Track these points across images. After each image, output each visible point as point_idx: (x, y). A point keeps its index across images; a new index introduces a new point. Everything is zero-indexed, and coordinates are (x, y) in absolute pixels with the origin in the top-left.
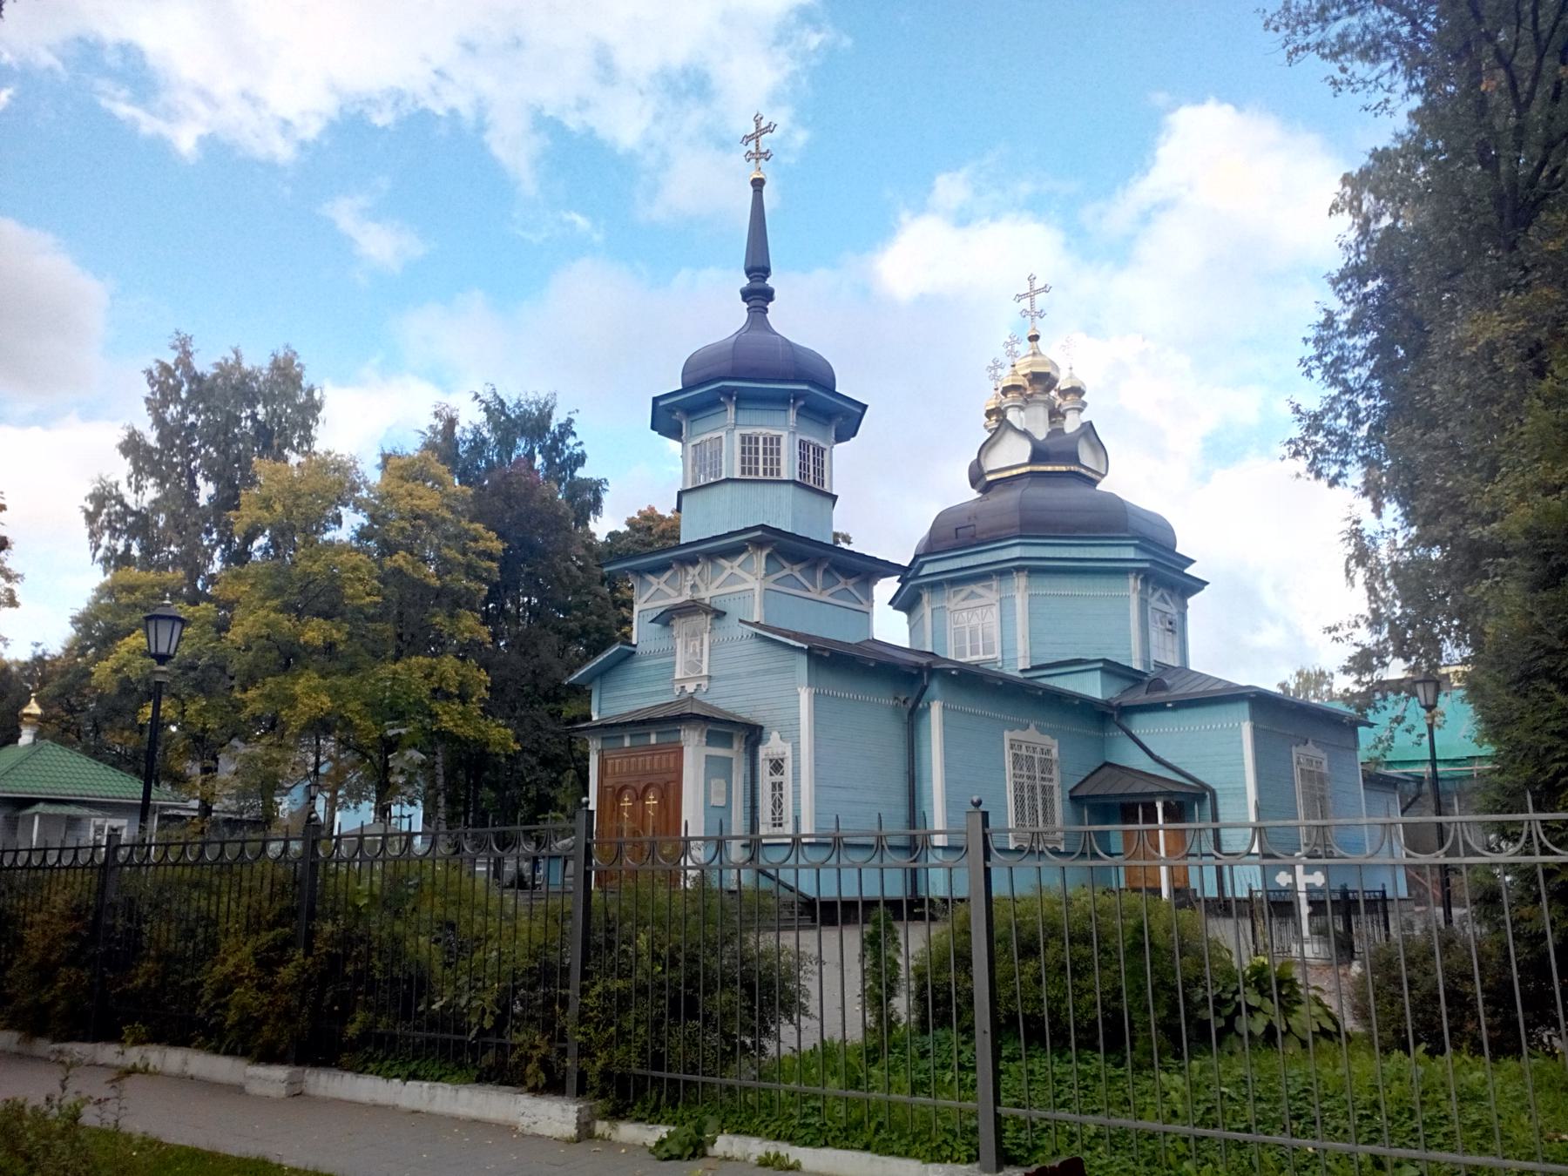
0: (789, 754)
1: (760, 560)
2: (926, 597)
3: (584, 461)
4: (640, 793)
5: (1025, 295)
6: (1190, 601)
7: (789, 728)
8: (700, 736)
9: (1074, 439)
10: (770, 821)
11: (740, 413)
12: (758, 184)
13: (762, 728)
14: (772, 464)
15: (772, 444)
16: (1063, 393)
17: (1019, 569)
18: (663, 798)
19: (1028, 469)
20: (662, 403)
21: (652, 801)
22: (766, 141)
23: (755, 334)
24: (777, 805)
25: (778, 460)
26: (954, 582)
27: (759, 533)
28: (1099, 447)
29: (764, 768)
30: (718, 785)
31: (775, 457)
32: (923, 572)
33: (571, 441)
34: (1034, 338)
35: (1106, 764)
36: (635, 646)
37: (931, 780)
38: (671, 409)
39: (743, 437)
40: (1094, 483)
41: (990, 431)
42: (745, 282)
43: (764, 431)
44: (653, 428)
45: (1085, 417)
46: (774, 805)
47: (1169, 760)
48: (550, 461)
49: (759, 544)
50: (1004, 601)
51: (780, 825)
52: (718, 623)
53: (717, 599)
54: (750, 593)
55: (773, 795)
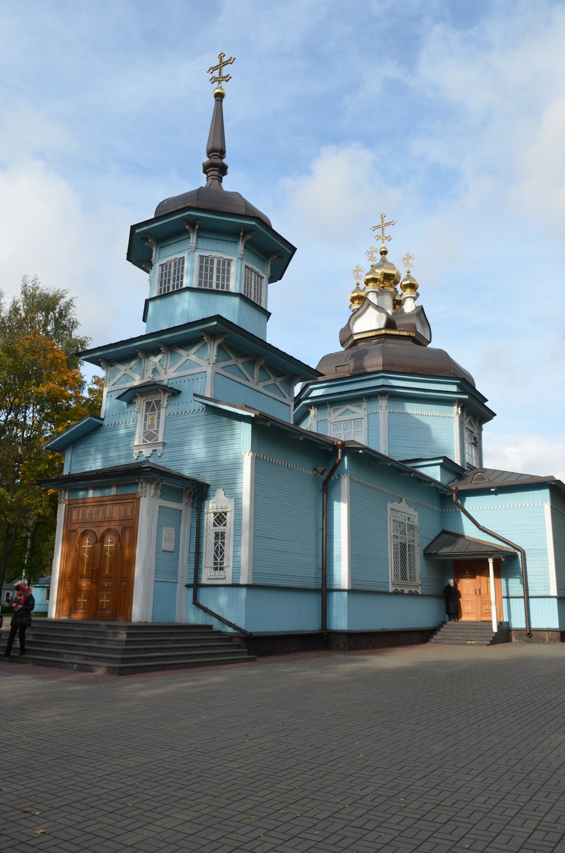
1: (212, 351)
2: (313, 412)
5: (378, 227)
6: (484, 426)
8: (156, 489)
10: (212, 565)
11: (201, 241)
12: (219, 97)
14: (223, 280)
15: (224, 265)
16: (405, 287)
17: (383, 394)
18: (120, 539)
19: (383, 332)
20: (137, 231)
22: (226, 71)
24: (219, 552)
27: (215, 323)
28: (426, 323)
29: (209, 518)
30: (168, 532)
31: (225, 283)
32: (311, 395)
34: (384, 253)
35: (444, 532)
36: (103, 419)
38: (144, 237)
40: (425, 346)
42: (206, 159)
43: (219, 255)
45: (419, 303)
46: (216, 552)
49: (213, 335)
51: (221, 569)
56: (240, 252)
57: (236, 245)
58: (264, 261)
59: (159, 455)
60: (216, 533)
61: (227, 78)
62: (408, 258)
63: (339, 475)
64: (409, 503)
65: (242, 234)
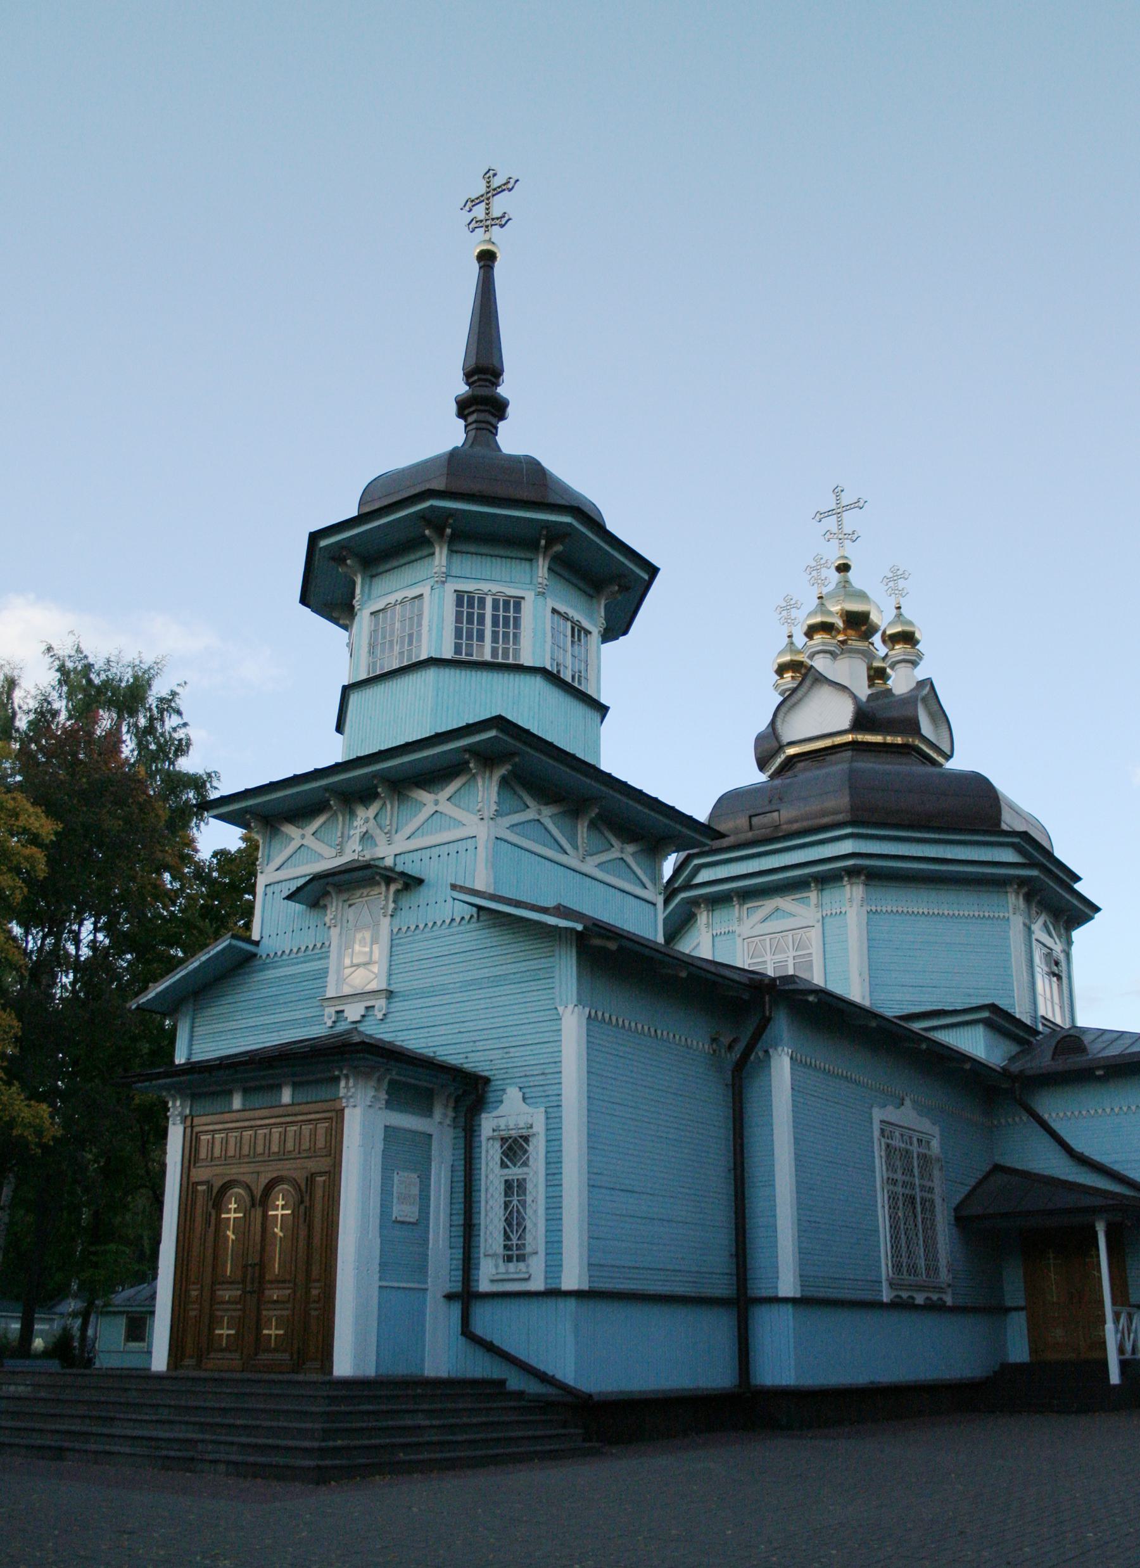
0: (539, 1127)
3: (188, 745)
4: (258, 1194)
6: (1076, 934)
7: (540, 1080)
9: (910, 700)
10: (500, 1250)
11: (456, 558)
12: (487, 259)
13: (487, 1081)
15: (506, 609)
17: (853, 873)
19: (849, 738)
20: (323, 543)
21: (280, 1210)
22: (500, 204)
23: (478, 450)
24: (514, 1222)
25: (517, 620)
26: (747, 895)
28: (940, 717)
29: (490, 1155)
30: (405, 1181)
32: (699, 879)
33: (171, 721)
35: (998, 1168)
36: (257, 943)
37: (771, 1184)
38: (338, 555)
39: (459, 595)
41: (781, 694)
42: (463, 389)
43: (495, 588)
44: (304, 600)
45: (920, 673)
47: (1097, 1157)
48: (141, 746)
49: (487, 758)
50: (827, 920)
52: (407, 900)
53: (408, 858)
54: (469, 844)
55: (506, 1205)
56: (540, 580)
57: (531, 565)
58: (591, 596)
59: (380, 1016)
60: (506, 1181)
61: (502, 221)
62: (895, 578)
63: (766, 1052)
64: (922, 1110)
65: (543, 542)
